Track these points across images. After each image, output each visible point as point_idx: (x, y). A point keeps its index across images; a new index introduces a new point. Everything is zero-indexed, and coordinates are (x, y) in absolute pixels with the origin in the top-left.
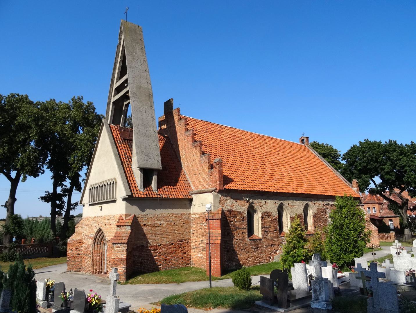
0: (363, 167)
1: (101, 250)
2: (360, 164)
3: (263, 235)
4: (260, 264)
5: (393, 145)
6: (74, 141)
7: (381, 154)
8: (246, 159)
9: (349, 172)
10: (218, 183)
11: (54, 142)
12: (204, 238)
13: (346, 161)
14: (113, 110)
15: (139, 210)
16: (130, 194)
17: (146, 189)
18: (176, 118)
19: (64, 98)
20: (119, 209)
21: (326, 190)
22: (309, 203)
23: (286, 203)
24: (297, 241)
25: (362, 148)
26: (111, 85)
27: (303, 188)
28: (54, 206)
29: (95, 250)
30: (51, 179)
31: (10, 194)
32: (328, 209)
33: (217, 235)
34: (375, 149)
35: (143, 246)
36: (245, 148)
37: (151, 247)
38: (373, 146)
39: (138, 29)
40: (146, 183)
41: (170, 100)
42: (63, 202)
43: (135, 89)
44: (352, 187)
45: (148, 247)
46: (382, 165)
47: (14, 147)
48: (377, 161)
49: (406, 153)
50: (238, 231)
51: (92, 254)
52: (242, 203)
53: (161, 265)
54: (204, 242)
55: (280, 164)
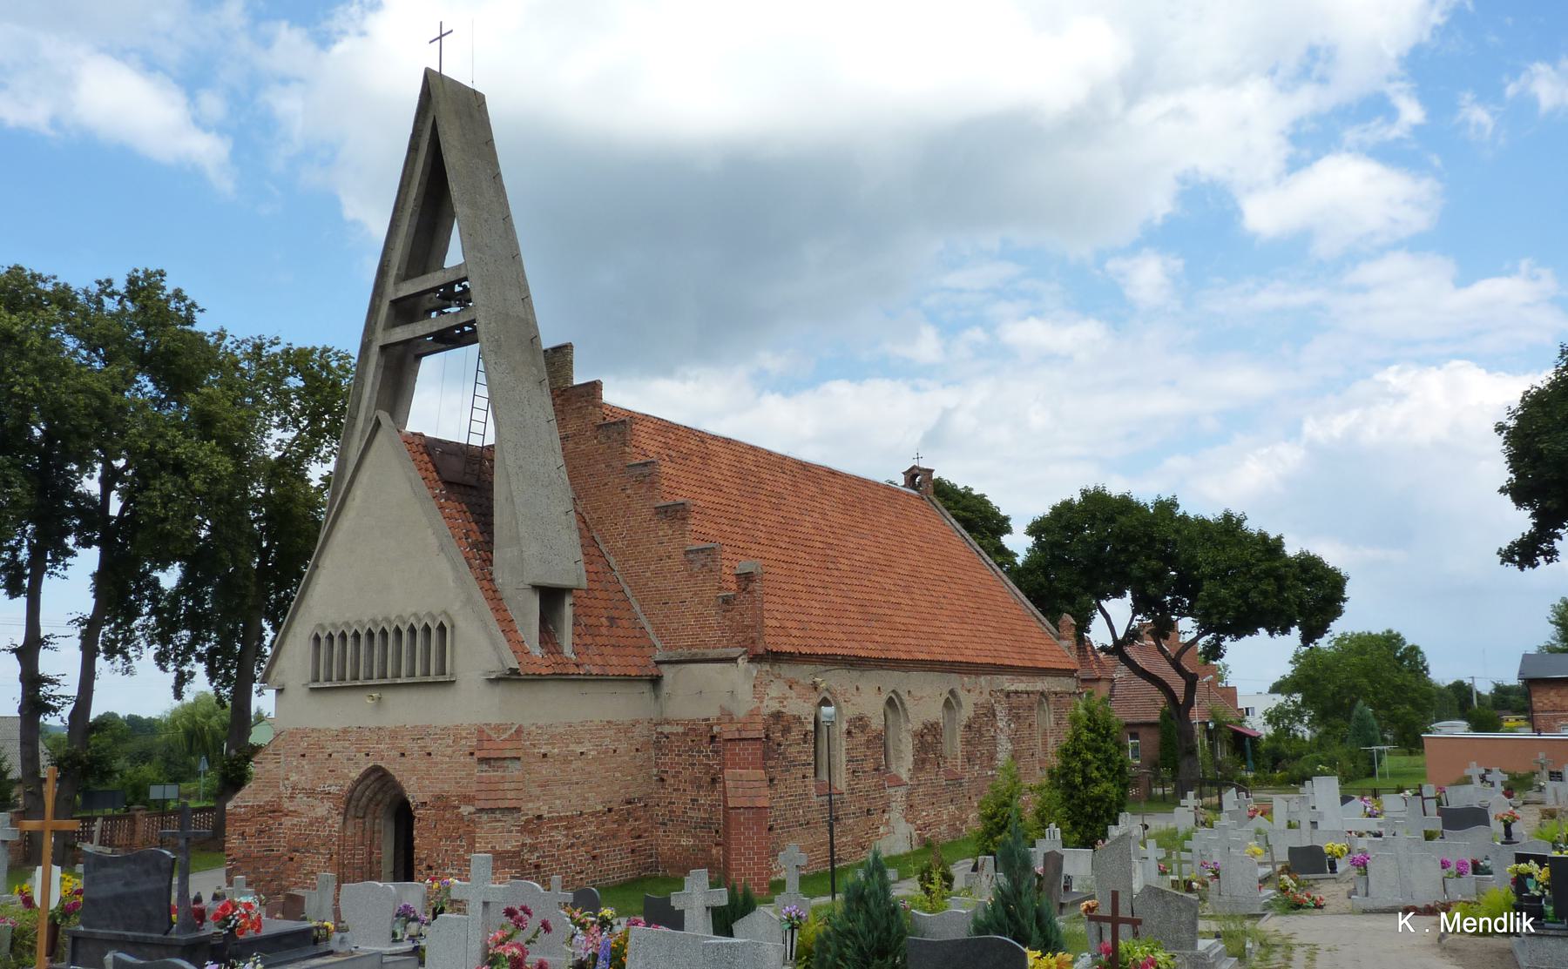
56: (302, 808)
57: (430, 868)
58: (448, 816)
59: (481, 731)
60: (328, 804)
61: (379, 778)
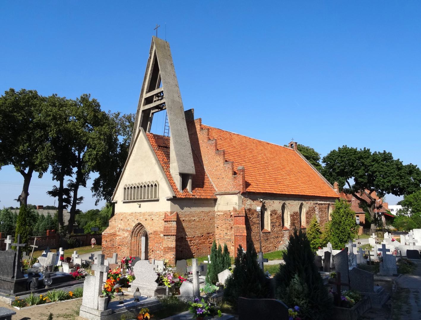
0: (341, 170)
1: (138, 241)
2: (339, 167)
3: (271, 230)
4: (269, 252)
5: (367, 151)
6: (87, 140)
7: (357, 160)
8: (255, 165)
9: (328, 174)
10: (242, 186)
11: (76, 143)
12: (228, 231)
13: (325, 163)
14: (142, 117)
15: (179, 208)
16: (175, 195)
17: (183, 191)
18: (198, 127)
19: (72, 95)
20: (164, 206)
21: (316, 191)
22: (304, 202)
23: (287, 202)
24: (316, 233)
25: (340, 153)
26: (141, 95)
27: (299, 190)
28: (61, 200)
29: (133, 241)
30: (51, 173)
31: (23, 189)
32: (317, 208)
33: (243, 229)
34: (352, 155)
35: (182, 238)
36: (251, 154)
37: (188, 238)
38: (351, 152)
39: (166, 45)
40: (184, 186)
41: (191, 109)
42: (70, 197)
43: (170, 103)
44: (334, 188)
45: (186, 238)
46: (357, 170)
47: (34, 145)
48: (353, 166)
49: (378, 160)
50: (255, 225)
51: (129, 245)
52: (258, 203)
53: (194, 253)
54: (229, 235)
55: (279, 168)
56: (121, 234)
57: (153, 251)
58: (157, 237)
59: (166, 213)
60: (128, 233)
61: (140, 225)
